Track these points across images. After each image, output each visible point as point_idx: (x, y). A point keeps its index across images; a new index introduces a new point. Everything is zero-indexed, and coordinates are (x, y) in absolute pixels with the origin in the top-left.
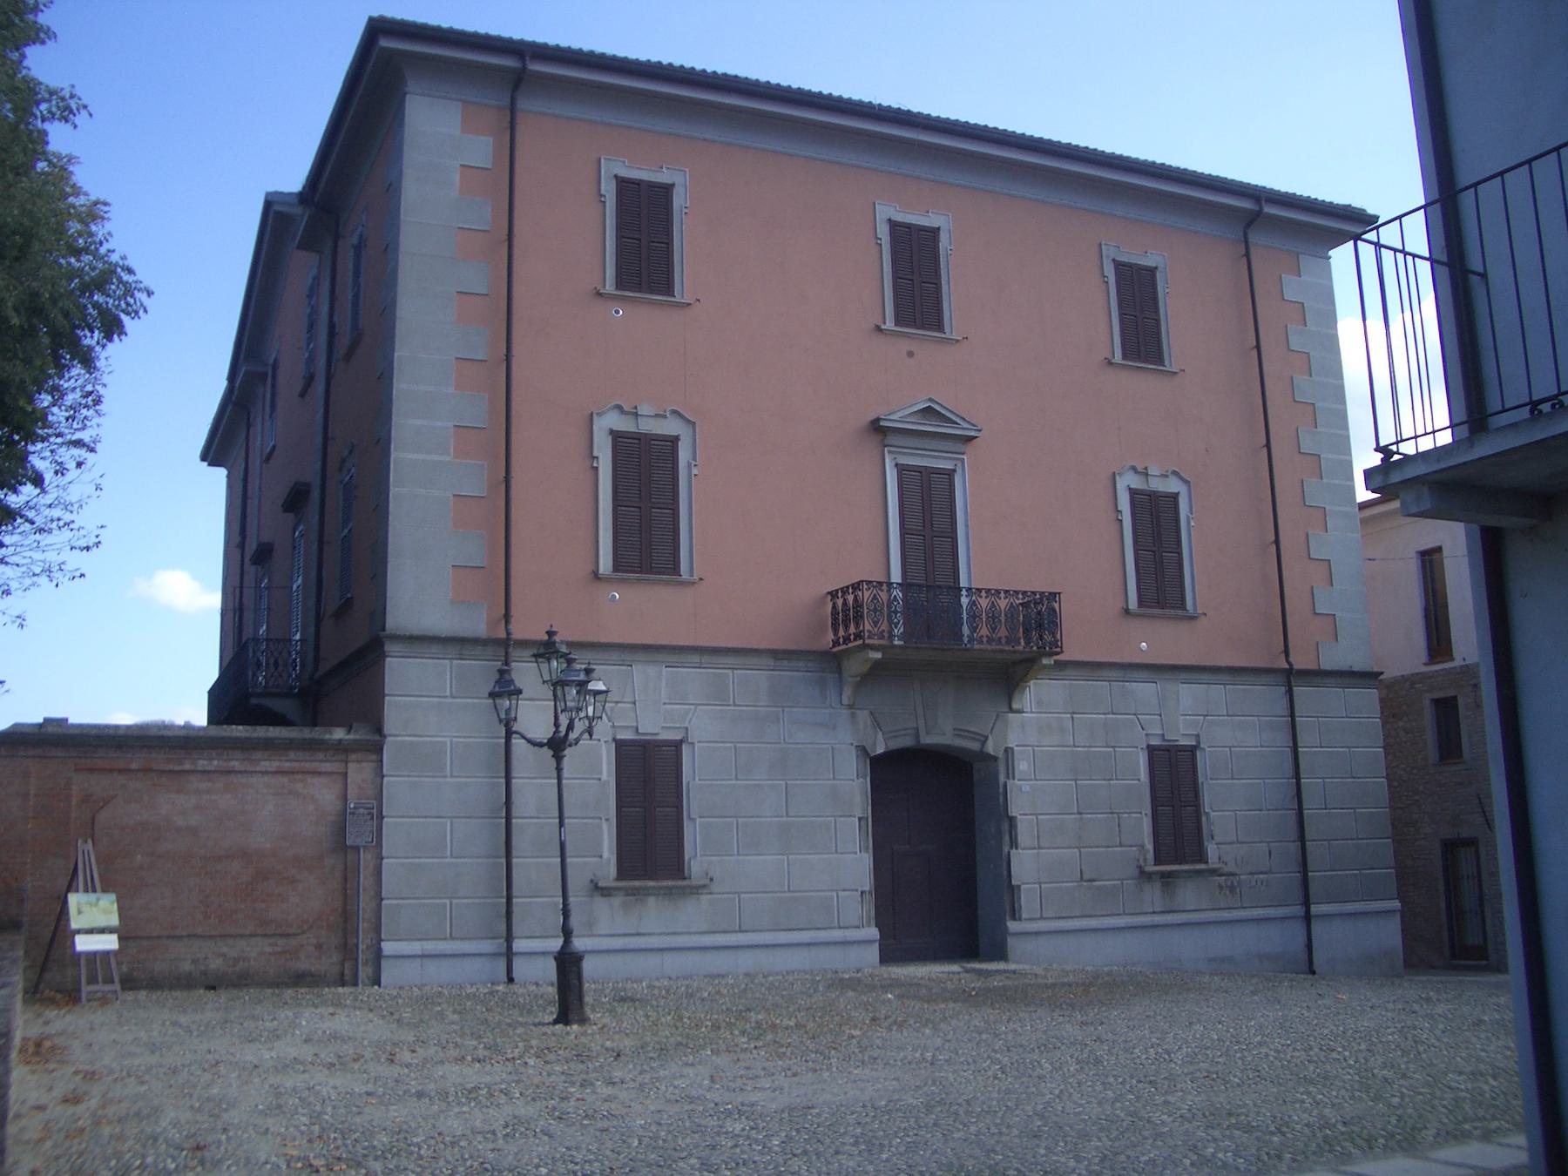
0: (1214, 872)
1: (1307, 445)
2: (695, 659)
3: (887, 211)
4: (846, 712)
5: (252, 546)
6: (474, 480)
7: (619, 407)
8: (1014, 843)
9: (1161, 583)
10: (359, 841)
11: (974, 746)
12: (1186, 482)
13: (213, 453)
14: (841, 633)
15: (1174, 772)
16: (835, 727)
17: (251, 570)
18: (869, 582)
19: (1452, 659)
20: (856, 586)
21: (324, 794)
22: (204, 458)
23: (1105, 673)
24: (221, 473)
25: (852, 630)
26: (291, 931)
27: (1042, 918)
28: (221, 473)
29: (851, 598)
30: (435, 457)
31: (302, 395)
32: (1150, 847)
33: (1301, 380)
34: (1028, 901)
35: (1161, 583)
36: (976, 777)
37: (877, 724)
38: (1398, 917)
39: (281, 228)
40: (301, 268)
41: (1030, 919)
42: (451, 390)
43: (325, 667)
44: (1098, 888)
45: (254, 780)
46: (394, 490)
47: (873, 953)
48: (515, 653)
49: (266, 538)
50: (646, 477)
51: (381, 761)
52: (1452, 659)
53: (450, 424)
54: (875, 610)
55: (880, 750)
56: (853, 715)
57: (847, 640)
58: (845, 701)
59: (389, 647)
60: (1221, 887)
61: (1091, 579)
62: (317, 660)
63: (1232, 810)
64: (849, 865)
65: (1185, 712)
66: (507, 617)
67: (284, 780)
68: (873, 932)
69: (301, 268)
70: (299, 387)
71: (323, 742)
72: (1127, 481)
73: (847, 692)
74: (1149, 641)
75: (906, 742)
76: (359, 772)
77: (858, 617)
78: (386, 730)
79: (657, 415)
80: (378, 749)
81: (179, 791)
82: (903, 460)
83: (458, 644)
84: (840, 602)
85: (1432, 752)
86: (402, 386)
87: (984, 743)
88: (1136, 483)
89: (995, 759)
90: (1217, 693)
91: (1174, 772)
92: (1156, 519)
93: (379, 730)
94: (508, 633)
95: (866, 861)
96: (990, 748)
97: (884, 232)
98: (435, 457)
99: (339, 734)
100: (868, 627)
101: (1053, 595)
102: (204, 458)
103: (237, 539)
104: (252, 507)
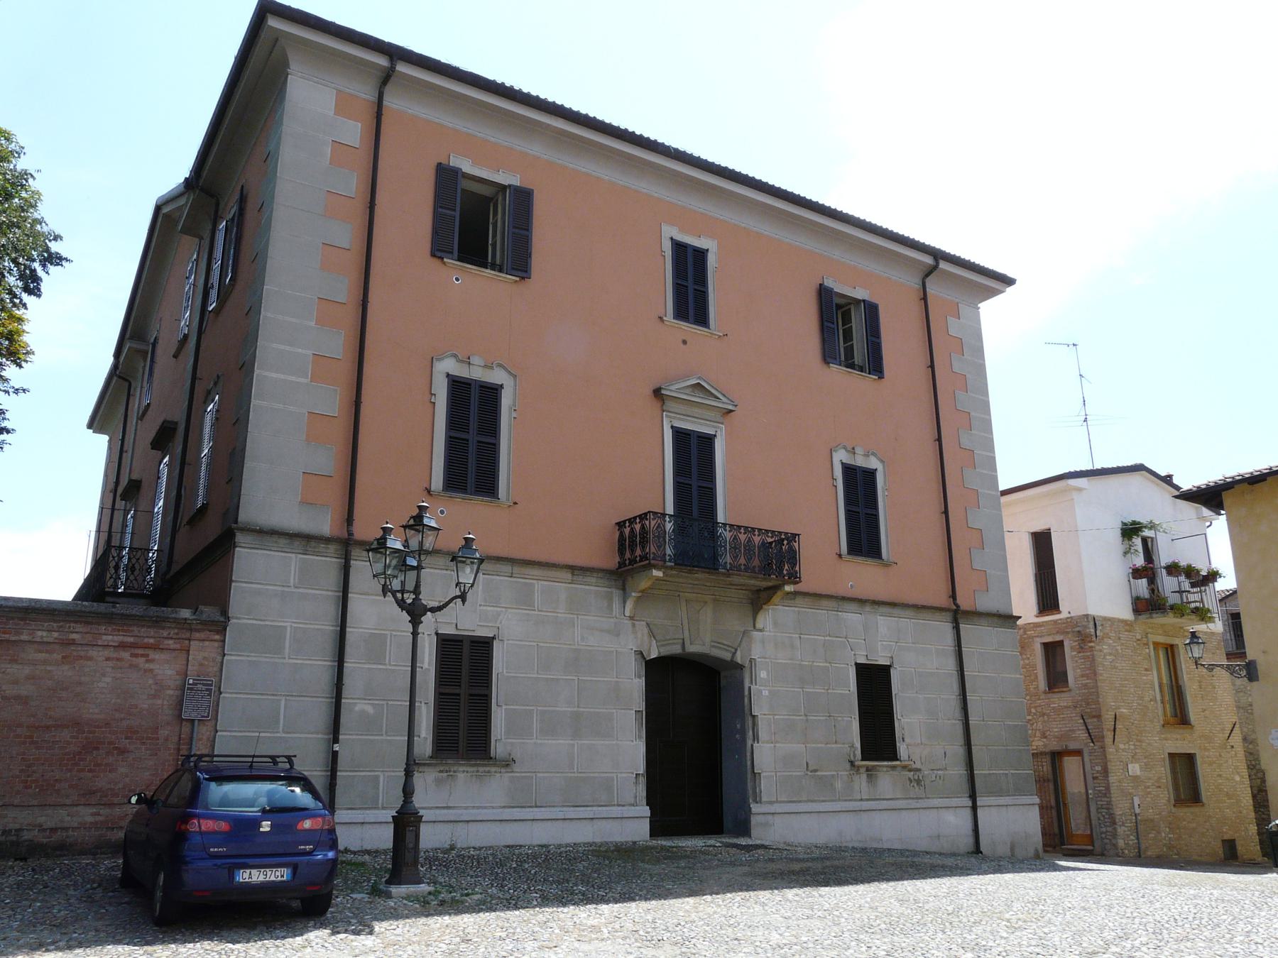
0: (904, 767)
1: (965, 442)
2: (507, 568)
3: (671, 232)
4: (629, 623)
5: (124, 482)
6: (330, 401)
7: (455, 356)
8: (756, 738)
9: (864, 538)
10: (193, 715)
11: (727, 656)
12: (882, 461)
13: (96, 423)
14: (628, 555)
15: (874, 684)
16: (618, 635)
17: (120, 504)
18: (655, 513)
19: (1059, 612)
20: (643, 517)
21: (165, 668)
22: (90, 426)
23: (825, 603)
24: (103, 439)
25: (638, 552)
26: (116, 800)
27: (777, 802)
28: (103, 439)
29: (638, 527)
30: (293, 378)
31: (175, 356)
32: (858, 745)
33: (961, 395)
34: (767, 786)
35: (864, 538)
36: (723, 682)
37: (652, 634)
38: (1037, 808)
39: (167, 224)
40: (187, 254)
41: (771, 803)
42: (313, 324)
43: (175, 568)
44: (821, 778)
45: (93, 653)
46: (254, 402)
47: (645, 827)
48: (356, 552)
49: (135, 476)
50: (474, 408)
51: (224, 641)
52: (1059, 612)
53: (310, 352)
54: (659, 537)
55: (653, 656)
56: (634, 625)
57: (633, 561)
58: (627, 614)
59: (239, 537)
60: (911, 781)
61: (820, 526)
62: (169, 564)
63: (919, 718)
64: (630, 751)
65: (882, 638)
66: (350, 520)
67: (125, 655)
68: (646, 811)
69: (187, 254)
70: (173, 351)
71: (166, 619)
72: (841, 456)
73: (629, 605)
74: (861, 576)
75: (676, 649)
76: (201, 651)
77: (644, 541)
78: (232, 612)
79: (486, 366)
80: (223, 631)
81: (13, 661)
82: (678, 424)
83: (306, 540)
84: (627, 531)
85: (1042, 684)
86: (268, 314)
87: (734, 654)
88: (848, 460)
89: (741, 667)
90: (908, 623)
91: (874, 684)
92: (860, 486)
93: (224, 612)
94: (350, 534)
95: (640, 748)
96: (739, 659)
97: (667, 247)
98: (293, 378)
99: (186, 613)
100: (653, 550)
101: (794, 535)
102: (90, 426)
103: (112, 486)
104: (127, 458)
